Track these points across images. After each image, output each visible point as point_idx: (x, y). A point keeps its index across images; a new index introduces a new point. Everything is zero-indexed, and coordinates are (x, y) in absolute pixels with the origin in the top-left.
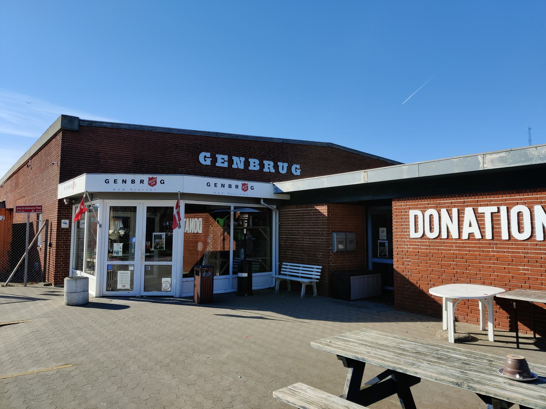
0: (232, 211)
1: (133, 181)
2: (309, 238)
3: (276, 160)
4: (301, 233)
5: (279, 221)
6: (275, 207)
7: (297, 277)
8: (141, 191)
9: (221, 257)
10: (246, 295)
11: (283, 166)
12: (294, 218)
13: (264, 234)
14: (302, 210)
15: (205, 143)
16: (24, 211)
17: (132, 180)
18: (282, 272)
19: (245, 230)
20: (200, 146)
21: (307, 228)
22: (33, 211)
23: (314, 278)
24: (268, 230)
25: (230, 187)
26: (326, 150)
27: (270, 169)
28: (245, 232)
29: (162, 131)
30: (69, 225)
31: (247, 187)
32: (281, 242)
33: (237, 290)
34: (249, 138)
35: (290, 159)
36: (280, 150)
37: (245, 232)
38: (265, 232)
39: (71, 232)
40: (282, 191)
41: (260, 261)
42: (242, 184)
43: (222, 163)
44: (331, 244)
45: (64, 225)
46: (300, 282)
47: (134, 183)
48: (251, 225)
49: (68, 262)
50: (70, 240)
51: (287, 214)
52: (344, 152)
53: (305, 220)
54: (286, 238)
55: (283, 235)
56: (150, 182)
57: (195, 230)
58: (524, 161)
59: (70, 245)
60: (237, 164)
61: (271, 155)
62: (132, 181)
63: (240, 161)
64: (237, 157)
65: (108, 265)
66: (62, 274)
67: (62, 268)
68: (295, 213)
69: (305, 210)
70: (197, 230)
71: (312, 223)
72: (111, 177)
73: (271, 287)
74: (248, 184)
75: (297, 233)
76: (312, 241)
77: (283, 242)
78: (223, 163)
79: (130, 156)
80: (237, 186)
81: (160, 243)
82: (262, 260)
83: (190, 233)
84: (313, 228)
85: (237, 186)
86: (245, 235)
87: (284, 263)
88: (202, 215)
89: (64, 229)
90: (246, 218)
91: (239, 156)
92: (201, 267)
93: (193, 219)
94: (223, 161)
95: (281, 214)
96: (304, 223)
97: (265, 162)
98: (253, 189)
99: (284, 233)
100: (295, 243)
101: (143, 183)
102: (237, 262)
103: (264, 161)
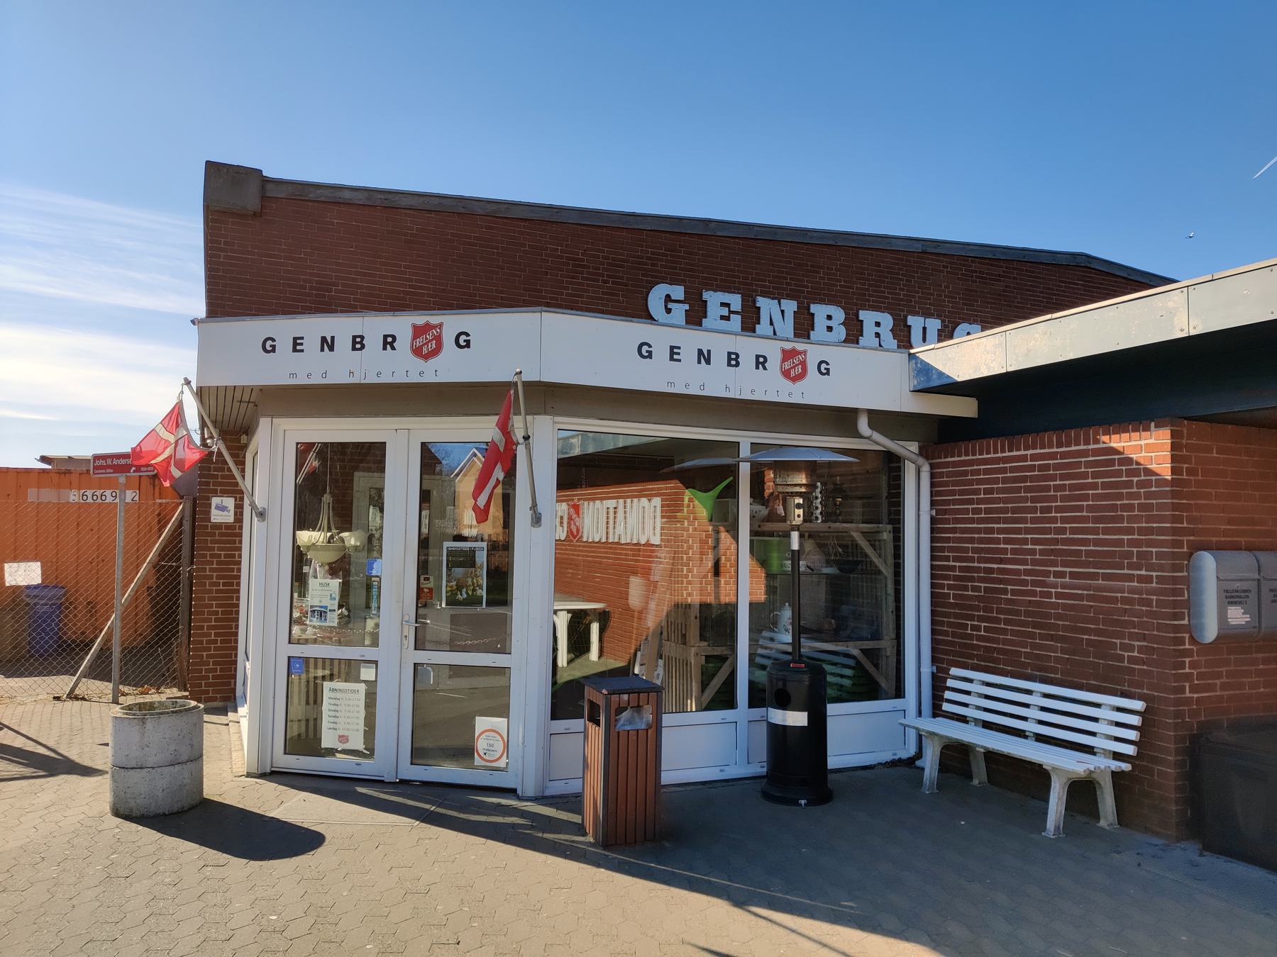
0: (745, 461)
1: (358, 340)
2: (1073, 575)
4: (1033, 552)
5: (933, 503)
6: (914, 447)
7: (1020, 733)
8: (386, 379)
10: (803, 802)
11: (924, 329)
12: (1000, 491)
13: (869, 550)
14: (1034, 457)
15: (666, 255)
16: (112, 471)
17: (354, 337)
19: (795, 536)
20: (653, 265)
22: (133, 469)
24: (886, 536)
25: (733, 362)
26: (1068, 278)
27: (882, 337)
28: (795, 546)
30: (236, 514)
32: (942, 586)
33: (765, 769)
34: (812, 238)
35: (948, 307)
36: (914, 277)
38: (873, 546)
39: (240, 535)
40: (948, 377)
41: (855, 652)
42: (784, 351)
43: (723, 318)
44: (1187, 604)
46: (1040, 766)
48: (817, 518)
49: (233, 630)
51: (965, 473)
52: (1127, 284)
55: (947, 558)
56: (419, 342)
57: (640, 535)
59: (239, 577)
60: (772, 323)
62: (354, 343)
63: (783, 312)
64: (773, 299)
65: (289, 657)
67: (215, 649)
69: (1053, 456)
71: (1090, 509)
72: (283, 328)
74: (805, 352)
75: (1014, 551)
76: (1088, 588)
77: (950, 587)
79: (429, 295)
83: (627, 544)
84: (1095, 531)
86: (796, 556)
87: (954, 671)
89: (218, 526)
91: (777, 295)
92: (605, 691)
93: (635, 500)
94: (725, 312)
95: (941, 475)
96: (1049, 510)
97: (863, 315)
98: (828, 373)
99: (951, 549)
100: (1005, 591)
101: (393, 348)
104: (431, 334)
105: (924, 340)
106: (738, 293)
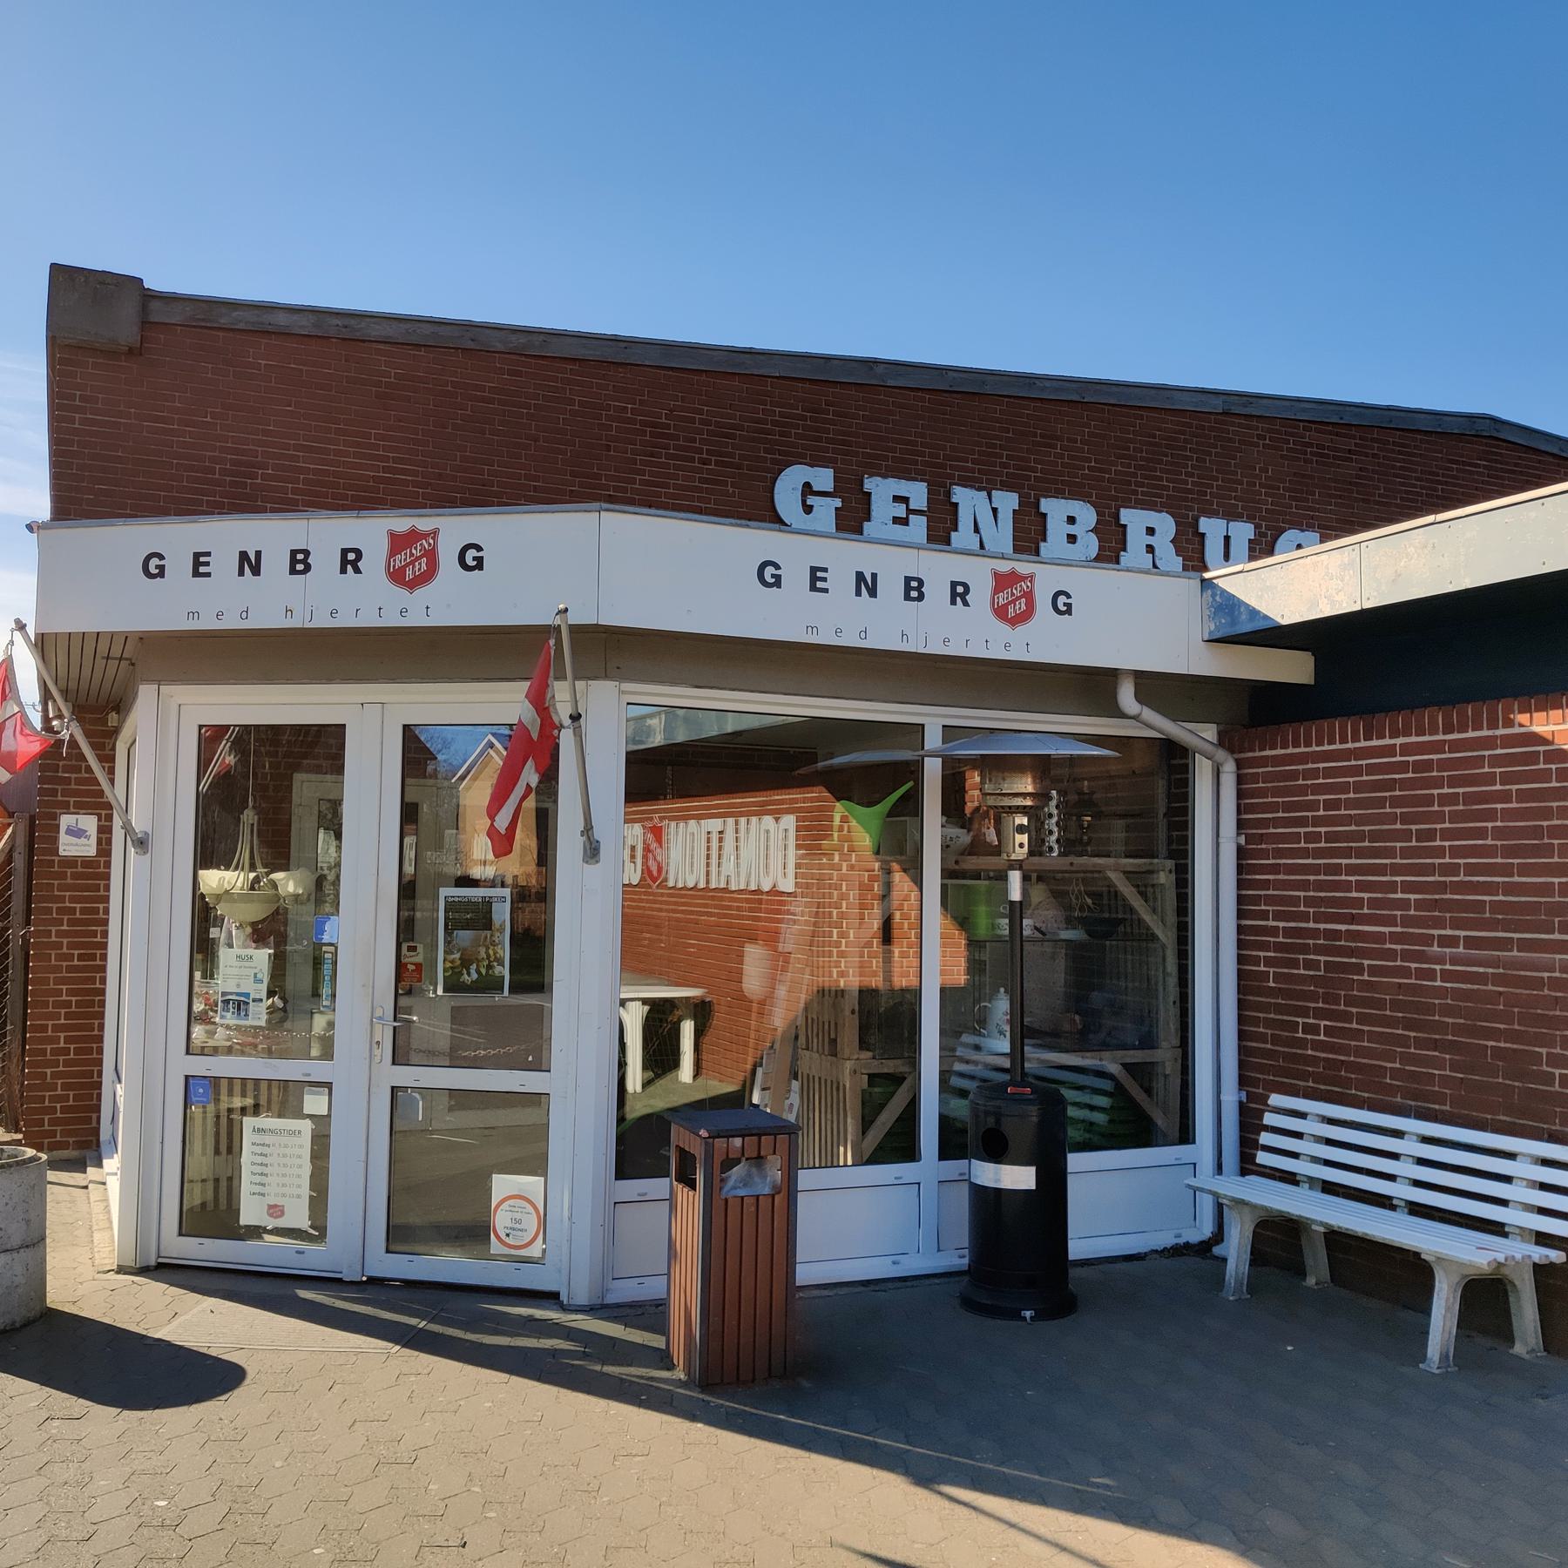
2: (1471, 943)
3: (1192, 509)
4: (1404, 904)
5: (1241, 825)
6: (1209, 732)
9: (863, 1045)
11: (1227, 539)
12: (1350, 804)
13: (1136, 902)
14: (1406, 749)
17: (294, 553)
18: (1262, 1158)
19: (1015, 877)
21: (1452, 870)
23: (1524, 1233)
24: (1165, 878)
25: (914, 594)
27: (1157, 552)
28: (1015, 894)
29: (581, 353)
31: (1029, 596)
34: (1043, 389)
37: (1015, 894)
38: (1143, 894)
40: (1266, 617)
42: (997, 576)
43: (896, 520)
45: (74, 840)
47: (308, 568)
48: (1051, 849)
49: (96, 1032)
50: (106, 922)
51: (1294, 775)
52: (1559, 465)
53: (1440, 817)
54: (1288, 932)
55: (1264, 915)
56: (399, 561)
60: (977, 530)
61: (1161, 479)
62: (294, 561)
63: (995, 510)
64: (979, 489)
65: (187, 1077)
66: (66, 1098)
68: (1357, 771)
70: (771, 874)
73: (1187, 1245)
74: (1031, 577)
75: (1373, 903)
76: (1495, 963)
77: (1269, 962)
78: (904, 522)
80: (960, 589)
81: (482, 951)
82: (1127, 1067)
84: (1506, 870)
85: (960, 589)
86: (1016, 911)
87: (1276, 1100)
88: (796, 801)
89: (71, 862)
90: (1019, 802)
91: (986, 484)
92: (703, 1133)
93: (754, 819)
94: (901, 511)
97: (1128, 516)
99: (1270, 900)
100: (1359, 969)
102: (972, 1077)
103: (1122, 510)
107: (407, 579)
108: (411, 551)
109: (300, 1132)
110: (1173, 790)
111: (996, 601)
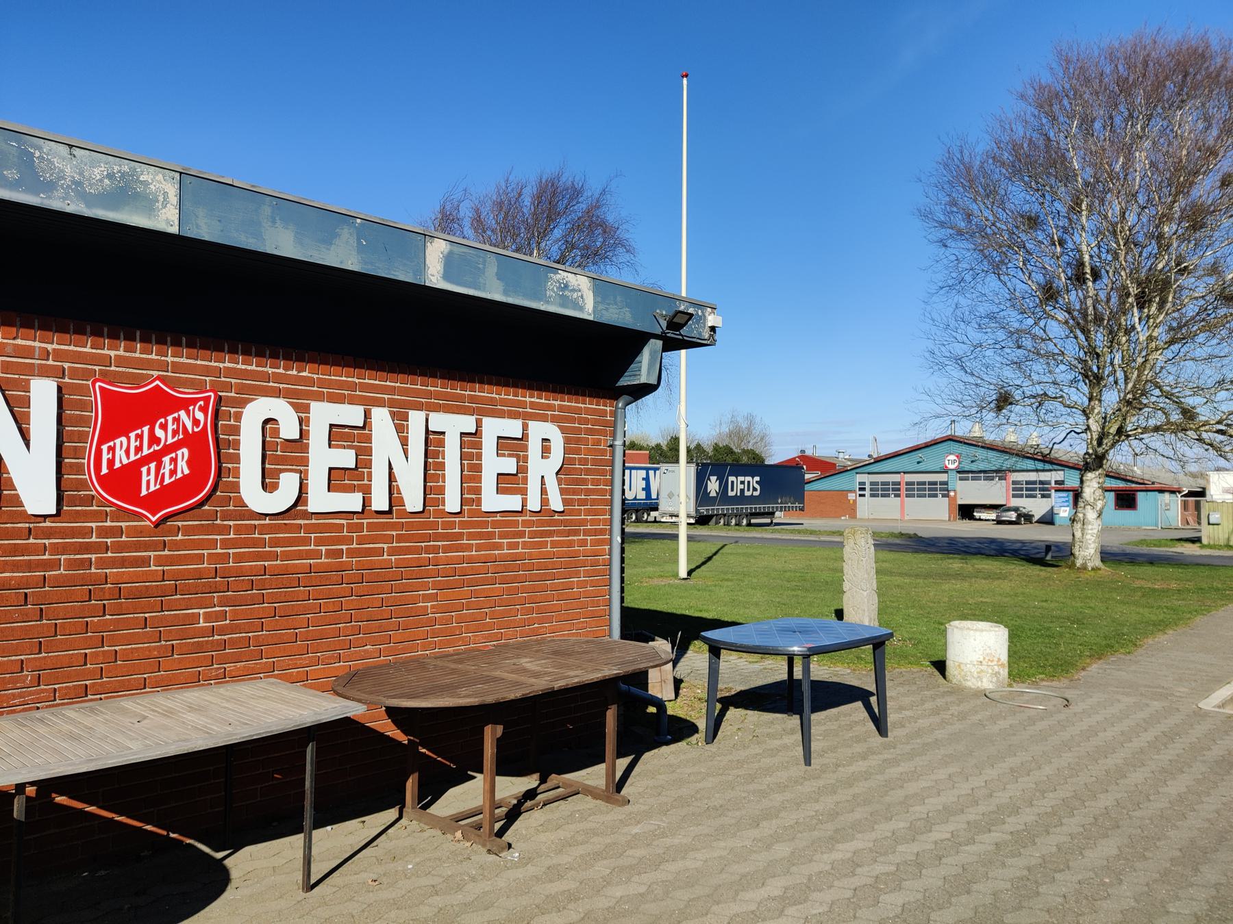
58: (387, 274)
104: (171, 427)
105: (677, 516)
106: (350, 447)
107: (144, 492)
108: (152, 432)
109: (545, 440)
110: (607, 547)
111: (105, 456)
